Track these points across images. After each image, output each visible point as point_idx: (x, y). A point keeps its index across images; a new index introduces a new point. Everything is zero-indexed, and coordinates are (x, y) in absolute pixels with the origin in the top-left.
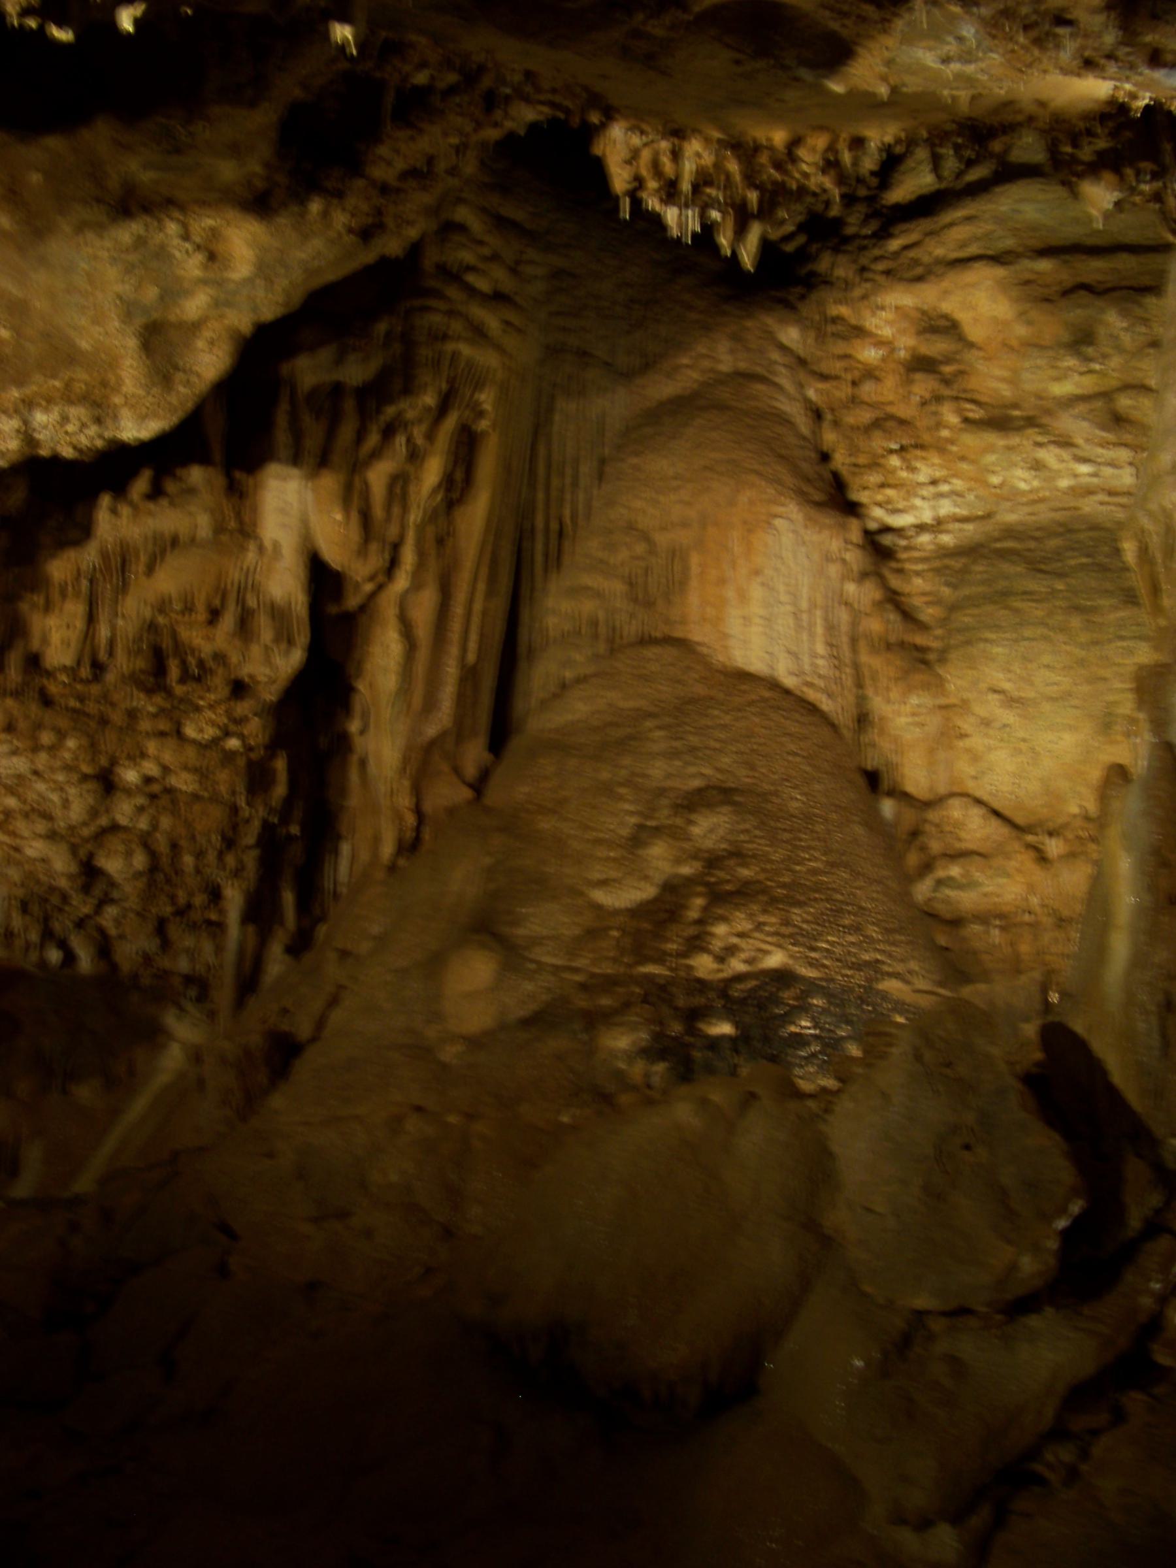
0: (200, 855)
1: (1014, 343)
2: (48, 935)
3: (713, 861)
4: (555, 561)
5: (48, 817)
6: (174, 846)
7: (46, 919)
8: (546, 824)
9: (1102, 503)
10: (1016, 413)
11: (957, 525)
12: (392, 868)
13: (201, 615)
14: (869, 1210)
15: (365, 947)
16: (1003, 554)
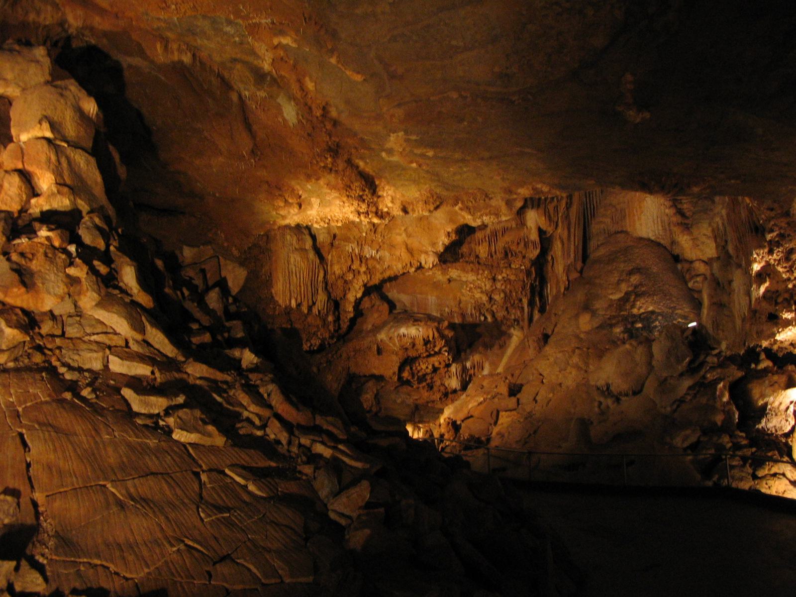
0: (516, 293)
2: (480, 313)
3: (636, 287)
4: (593, 215)
5: (481, 288)
6: (511, 291)
7: (480, 310)
8: (597, 281)
12: (564, 294)
13: (515, 244)
15: (560, 313)
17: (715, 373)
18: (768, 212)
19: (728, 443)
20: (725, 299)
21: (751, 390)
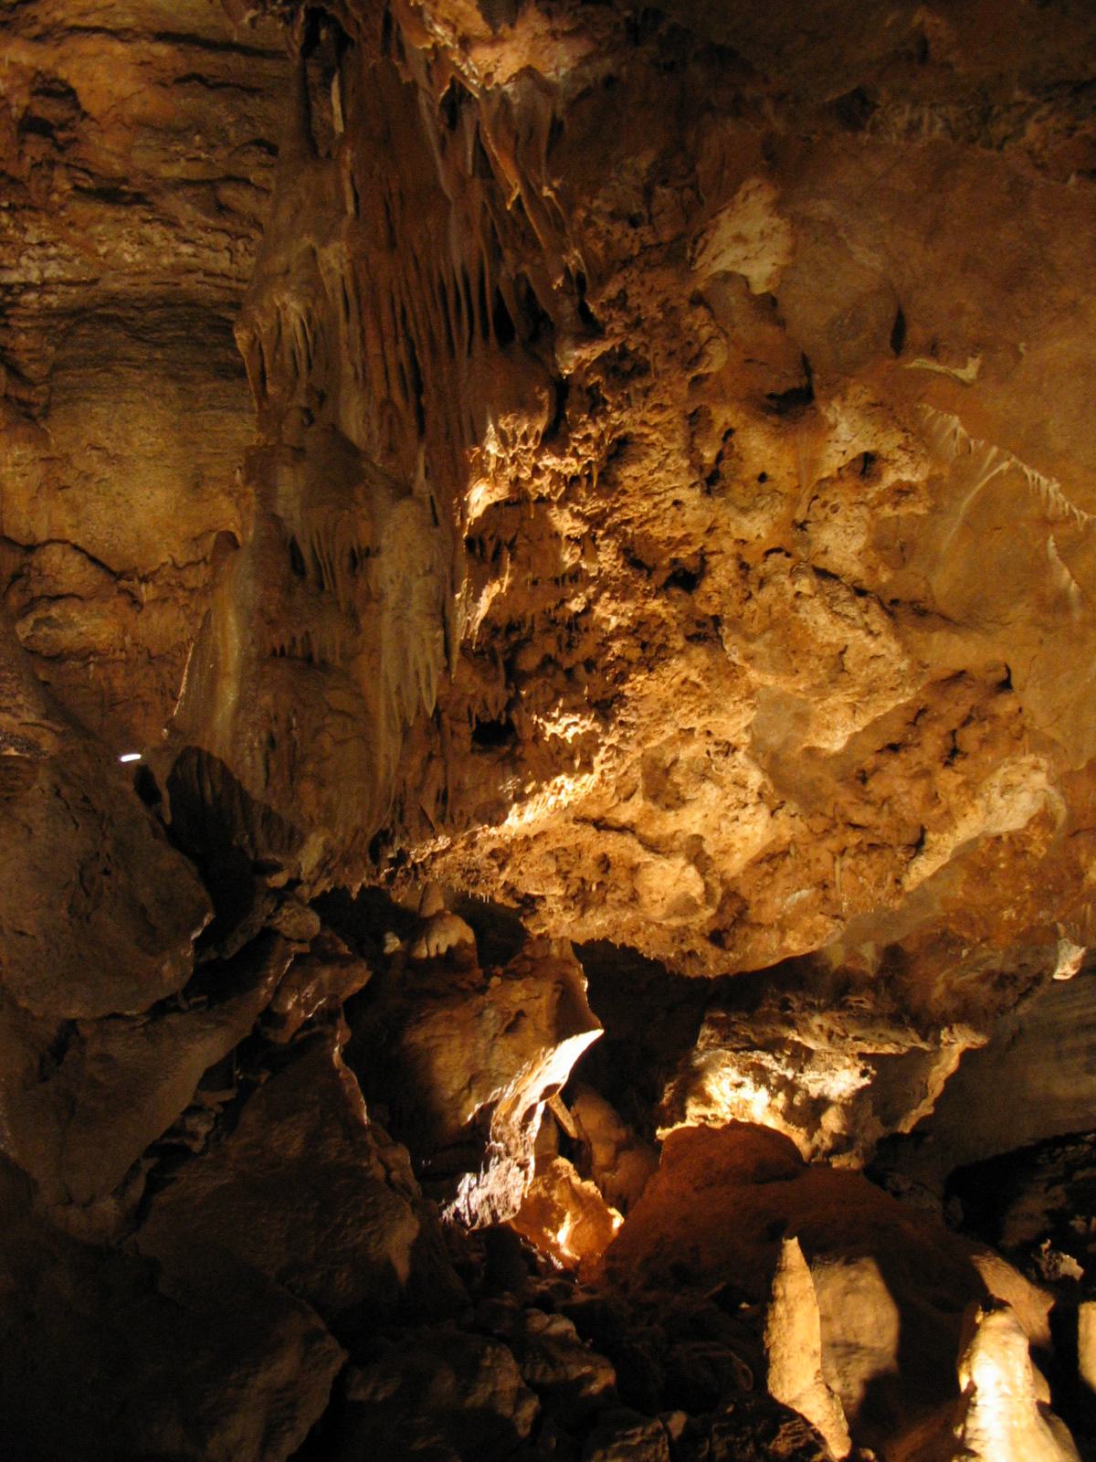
1: (127, 120)
9: (198, 282)
10: (124, 188)
11: (61, 288)
14: (22, 933)
16: (107, 320)
17: (309, 991)
18: (618, 230)
19: (520, 1396)
20: (328, 636)
21: (431, 1052)
